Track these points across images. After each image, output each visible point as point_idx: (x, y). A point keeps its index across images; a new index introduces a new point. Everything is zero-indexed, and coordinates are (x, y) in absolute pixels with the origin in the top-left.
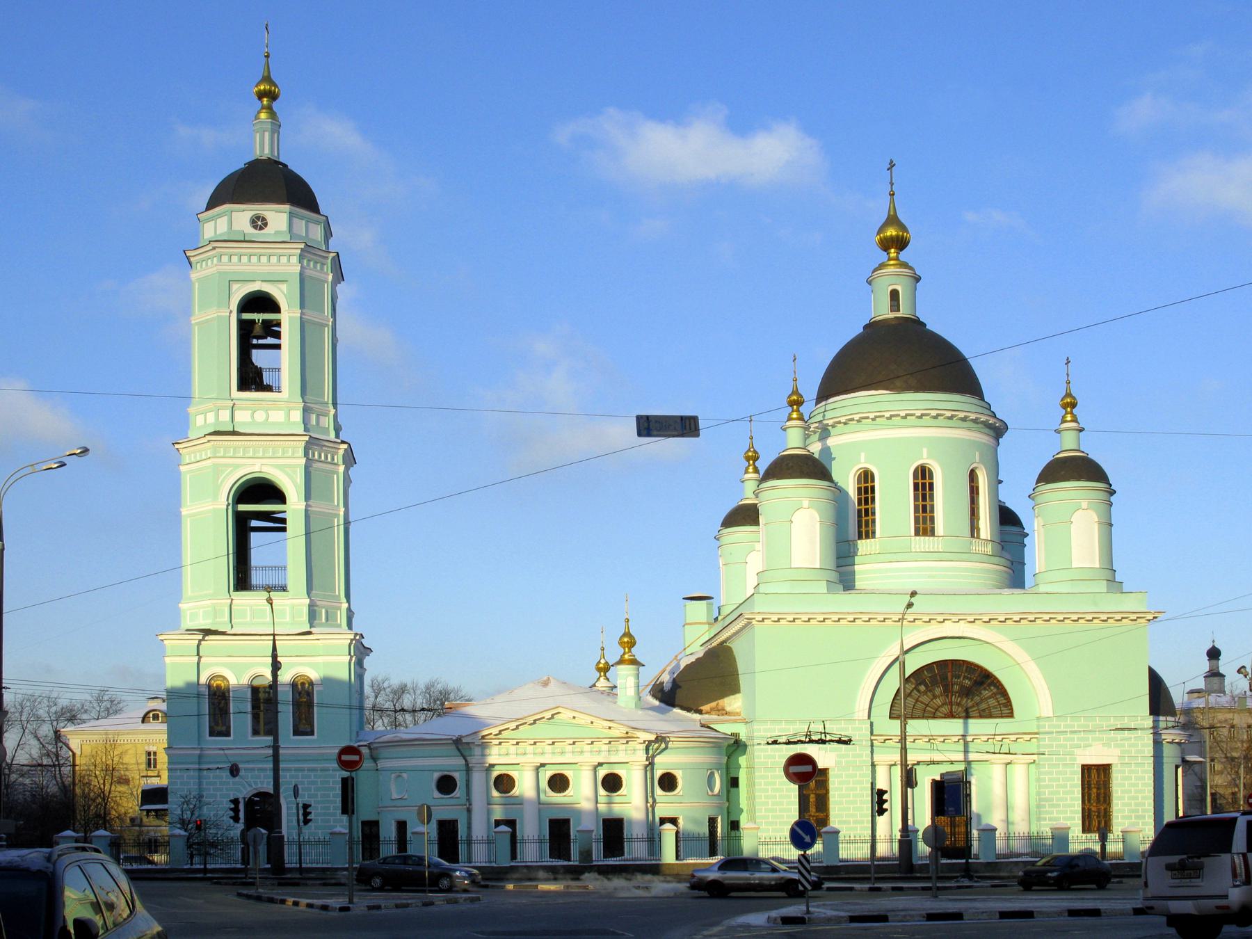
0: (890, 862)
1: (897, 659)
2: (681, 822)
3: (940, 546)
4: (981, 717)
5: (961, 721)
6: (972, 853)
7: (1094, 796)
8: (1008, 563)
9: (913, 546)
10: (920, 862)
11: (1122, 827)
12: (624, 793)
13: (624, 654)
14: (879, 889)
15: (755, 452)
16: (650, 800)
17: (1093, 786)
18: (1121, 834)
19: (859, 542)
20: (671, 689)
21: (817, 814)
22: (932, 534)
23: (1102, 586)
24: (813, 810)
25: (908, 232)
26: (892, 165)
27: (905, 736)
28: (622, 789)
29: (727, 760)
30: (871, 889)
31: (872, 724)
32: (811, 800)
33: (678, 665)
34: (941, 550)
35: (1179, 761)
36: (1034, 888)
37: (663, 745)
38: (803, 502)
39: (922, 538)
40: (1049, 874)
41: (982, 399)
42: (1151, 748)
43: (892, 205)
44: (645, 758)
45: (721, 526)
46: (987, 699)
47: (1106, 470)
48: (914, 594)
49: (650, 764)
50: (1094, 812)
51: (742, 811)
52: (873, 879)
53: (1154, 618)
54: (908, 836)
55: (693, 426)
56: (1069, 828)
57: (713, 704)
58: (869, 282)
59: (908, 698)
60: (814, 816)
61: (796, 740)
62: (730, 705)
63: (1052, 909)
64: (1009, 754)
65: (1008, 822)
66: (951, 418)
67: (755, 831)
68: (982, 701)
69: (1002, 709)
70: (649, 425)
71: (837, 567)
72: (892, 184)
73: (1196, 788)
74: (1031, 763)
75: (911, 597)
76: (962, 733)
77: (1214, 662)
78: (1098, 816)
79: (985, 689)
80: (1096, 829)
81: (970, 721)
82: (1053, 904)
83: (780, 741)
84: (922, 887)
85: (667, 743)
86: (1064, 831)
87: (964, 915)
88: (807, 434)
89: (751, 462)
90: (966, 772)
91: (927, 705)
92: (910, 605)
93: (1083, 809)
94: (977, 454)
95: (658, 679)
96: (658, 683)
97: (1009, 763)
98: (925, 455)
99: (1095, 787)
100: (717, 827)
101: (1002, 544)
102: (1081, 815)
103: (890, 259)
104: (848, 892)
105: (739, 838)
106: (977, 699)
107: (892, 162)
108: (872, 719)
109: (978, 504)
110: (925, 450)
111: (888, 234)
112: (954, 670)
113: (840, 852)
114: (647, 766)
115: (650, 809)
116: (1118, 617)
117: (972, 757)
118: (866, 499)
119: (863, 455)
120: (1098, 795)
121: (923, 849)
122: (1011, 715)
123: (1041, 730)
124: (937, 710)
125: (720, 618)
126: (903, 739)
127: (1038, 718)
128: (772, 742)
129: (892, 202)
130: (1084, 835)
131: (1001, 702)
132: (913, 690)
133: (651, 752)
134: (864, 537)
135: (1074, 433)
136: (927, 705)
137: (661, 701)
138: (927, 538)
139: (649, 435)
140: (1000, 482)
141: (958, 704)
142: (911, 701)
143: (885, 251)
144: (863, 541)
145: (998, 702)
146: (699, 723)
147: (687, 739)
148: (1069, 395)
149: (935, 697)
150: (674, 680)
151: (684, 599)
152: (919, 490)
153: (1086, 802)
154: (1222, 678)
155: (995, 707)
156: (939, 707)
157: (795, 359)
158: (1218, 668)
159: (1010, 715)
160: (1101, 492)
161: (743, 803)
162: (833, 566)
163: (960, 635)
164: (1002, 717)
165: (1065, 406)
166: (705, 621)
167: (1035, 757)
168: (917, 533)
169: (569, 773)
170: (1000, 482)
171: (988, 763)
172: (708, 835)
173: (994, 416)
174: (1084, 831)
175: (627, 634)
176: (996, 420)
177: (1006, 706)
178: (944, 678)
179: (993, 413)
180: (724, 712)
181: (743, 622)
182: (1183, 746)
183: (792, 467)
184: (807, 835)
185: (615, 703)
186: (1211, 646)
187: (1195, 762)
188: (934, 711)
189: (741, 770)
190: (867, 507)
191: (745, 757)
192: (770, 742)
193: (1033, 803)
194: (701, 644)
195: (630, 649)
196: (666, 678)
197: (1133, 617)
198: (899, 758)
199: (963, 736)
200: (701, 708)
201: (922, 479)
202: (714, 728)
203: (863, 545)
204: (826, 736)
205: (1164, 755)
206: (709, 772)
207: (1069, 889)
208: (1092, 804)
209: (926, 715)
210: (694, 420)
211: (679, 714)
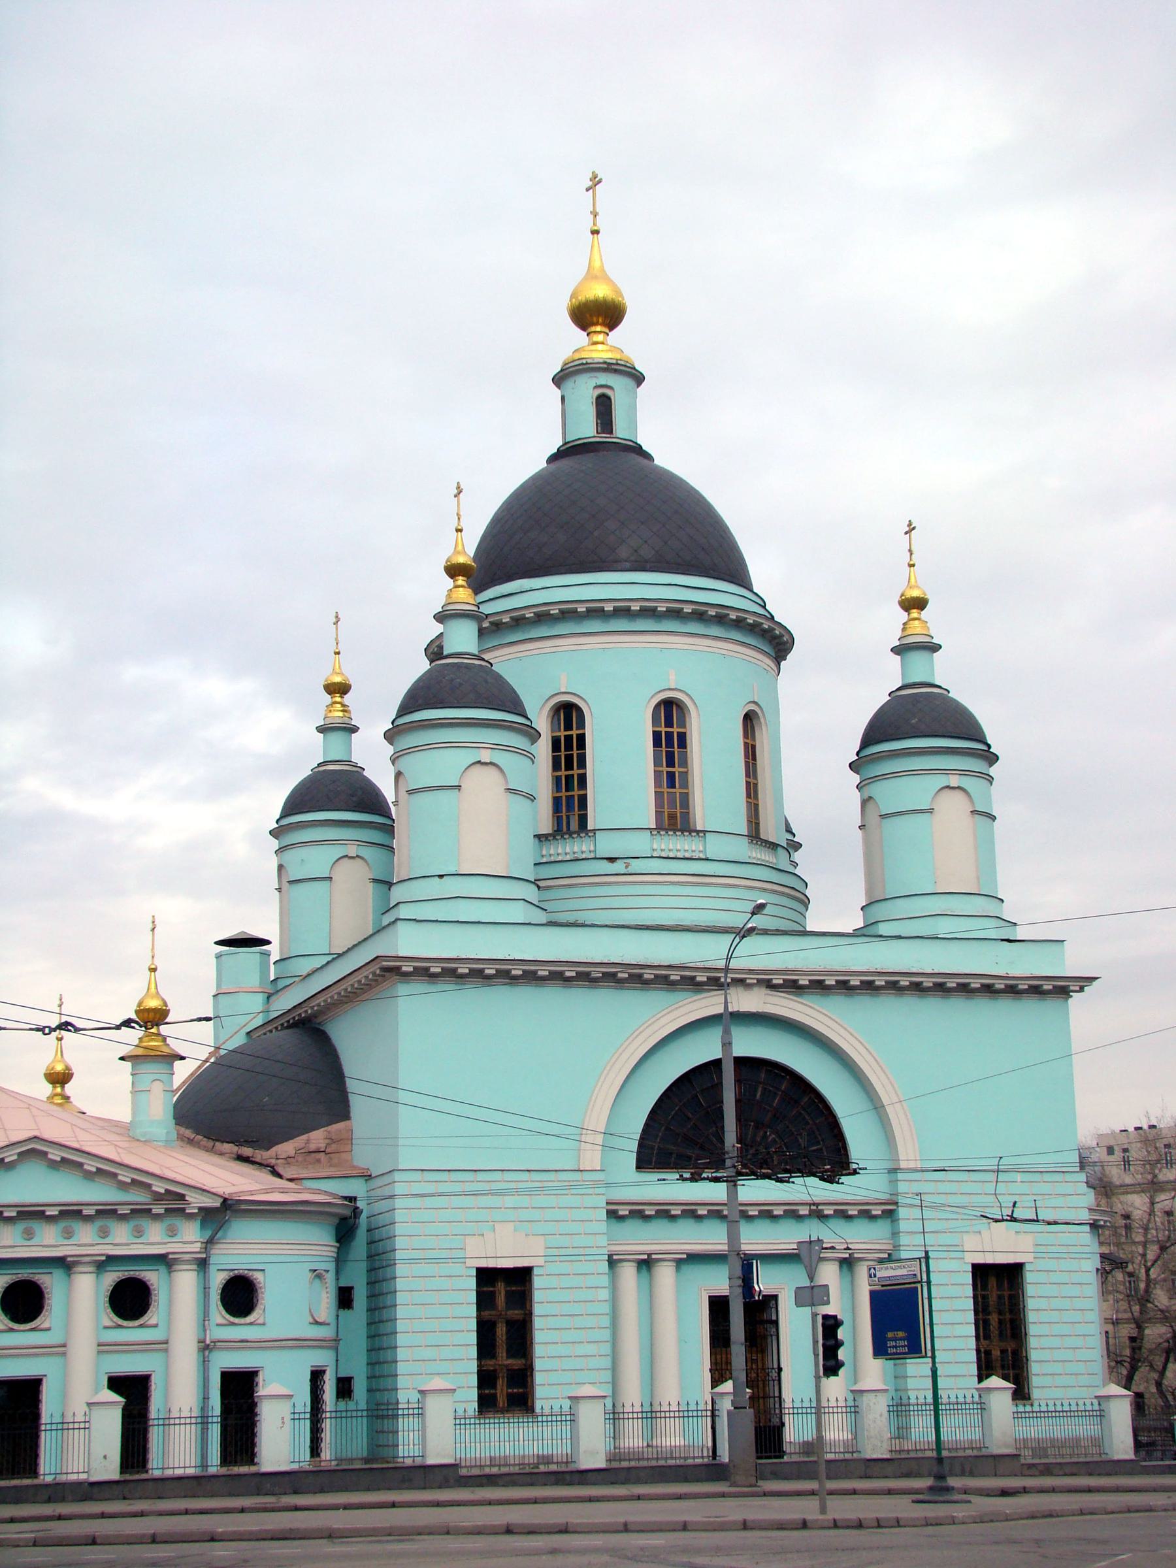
12: (153, 1321)
18: (977, 1393)
24: (502, 1352)
26: (596, 181)
28: (149, 1313)
72: (595, 214)
107: (595, 176)
151: (220, 943)
157: (460, 492)
190: (570, 772)
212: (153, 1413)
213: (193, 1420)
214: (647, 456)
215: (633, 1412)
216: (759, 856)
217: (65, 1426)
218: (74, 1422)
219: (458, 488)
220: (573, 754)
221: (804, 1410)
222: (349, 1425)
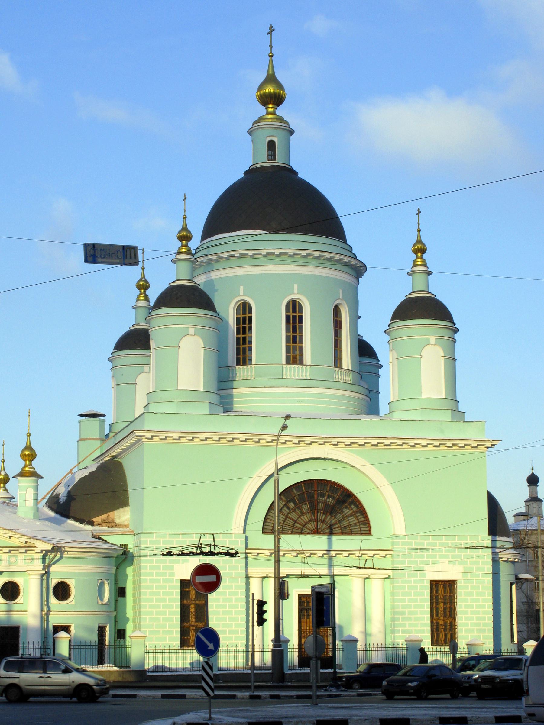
0: (263, 671)
1: (272, 475)
2: (72, 629)
3: (308, 374)
4: (343, 533)
5: (326, 537)
7: (441, 610)
8: (366, 392)
9: (284, 373)
10: (290, 672)
13: (25, 466)
14: (258, 697)
15: (146, 281)
16: (45, 608)
17: (440, 601)
18: (466, 647)
19: (237, 367)
20: (66, 500)
21: (197, 624)
22: (301, 363)
23: (447, 415)
24: (192, 619)
25: (284, 90)
26: (271, 30)
27: (279, 550)
28: (20, 597)
29: (116, 570)
30: (252, 697)
31: (247, 538)
32: (191, 610)
33: (73, 478)
35: (513, 579)
36: (396, 697)
37: (59, 555)
38: (190, 329)
39: (293, 366)
40: (410, 684)
41: (345, 242)
42: (490, 566)
43: (270, 65)
44: (42, 567)
45: (114, 349)
46: (348, 517)
48: (288, 417)
49: (46, 573)
50: (442, 625)
51: (128, 620)
52: (253, 687)
53: (493, 445)
54: (280, 646)
55: (133, 256)
56: (422, 640)
57: (104, 516)
60: (193, 626)
61: (188, 552)
62: (120, 517)
63: (426, 717)
64: (373, 568)
65: (366, 634)
66: (318, 258)
67: (142, 640)
68: (344, 518)
69: (362, 526)
70: (95, 252)
71: (218, 390)
72: (271, 47)
73: (523, 605)
74: (387, 578)
75: (285, 420)
76: (326, 548)
77: (533, 487)
78: (445, 630)
79: (346, 508)
80: (443, 642)
81: (334, 537)
82: (422, 712)
83: (174, 552)
84: (297, 696)
85: (62, 553)
86: (417, 642)
87: (349, 721)
88: (193, 267)
89: (142, 291)
90: (332, 586)
92: (284, 428)
93: (432, 622)
94: (341, 291)
95: (54, 491)
96: (54, 495)
97: (367, 578)
98: (296, 291)
99: (442, 602)
100: (105, 636)
101: (360, 373)
102: (430, 628)
103: (268, 113)
104: (231, 700)
105: (124, 647)
106: (339, 516)
107: (271, 27)
108: (247, 533)
109: (341, 337)
110: (296, 286)
111: (267, 91)
112: (319, 489)
113: (219, 661)
114: (43, 574)
115: (45, 617)
116: (461, 444)
117: (336, 571)
118: (244, 329)
119: (242, 288)
120: (445, 609)
121: (293, 656)
122: (369, 533)
123: (395, 547)
124: (304, 526)
125: (111, 435)
126: (276, 552)
127: (393, 536)
128: (167, 553)
129: (271, 63)
130: (435, 647)
131: (360, 520)
132: (283, 507)
133: (47, 561)
134: (241, 364)
135: (423, 276)
137: (57, 512)
138: (297, 366)
139: (94, 262)
140: (359, 317)
141: (323, 521)
142: (282, 517)
143: (264, 106)
144: (241, 367)
145: (358, 520)
146: (91, 534)
147: (80, 550)
148: (419, 241)
149: (303, 514)
150: (69, 492)
151: (79, 415)
152: (290, 323)
153: (435, 615)
154: (540, 503)
156: (306, 523)
157: (185, 199)
158: (537, 493)
159: (368, 532)
160: (447, 329)
161: (130, 613)
162: (213, 388)
163: (326, 457)
165: (416, 251)
166: (98, 437)
167: (390, 572)
168: (288, 362)
169: (19, 581)
170: (359, 317)
171: (348, 577)
172: (97, 644)
173: (355, 257)
174: (432, 644)
175: (29, 447)
176: (356, 262)
177: (364, 524)
178: (311, 497)
179: (355, 255)
180: (114, 524)
181: (133, 439)
182: (516, 564)
183: (181, 296)
184: (211, 643)
185: (15, 513)
186: (531, 473)
187: (527, 580)
188: (302, 527)
189: (128, 579)
191: (131, 567)
192: (165, 553)
193: (389, 616)
194: (93, 459)
195: (31, 461)
196: (62, 491)
197: (474, 444)
198: (273, 571)
199: (327, 551)
200: (93, 520)
201: (293, 312)
202: (105, 539)
203: (242, 371)
204: (215, 549)
205: (501, 573)
206: (100, 581)
207: (426, 699)
208: (439, 619)
209: (294, 530)
210: (134, 249)
211: (73, 525)
212: (21, 644)
213: (39, 647)
214: (296, 173)
215: (369, 648)
216: (108, 457)
217: (25, 648)
218: (28, 646)
219: (185, 196)
220: (246, 326)
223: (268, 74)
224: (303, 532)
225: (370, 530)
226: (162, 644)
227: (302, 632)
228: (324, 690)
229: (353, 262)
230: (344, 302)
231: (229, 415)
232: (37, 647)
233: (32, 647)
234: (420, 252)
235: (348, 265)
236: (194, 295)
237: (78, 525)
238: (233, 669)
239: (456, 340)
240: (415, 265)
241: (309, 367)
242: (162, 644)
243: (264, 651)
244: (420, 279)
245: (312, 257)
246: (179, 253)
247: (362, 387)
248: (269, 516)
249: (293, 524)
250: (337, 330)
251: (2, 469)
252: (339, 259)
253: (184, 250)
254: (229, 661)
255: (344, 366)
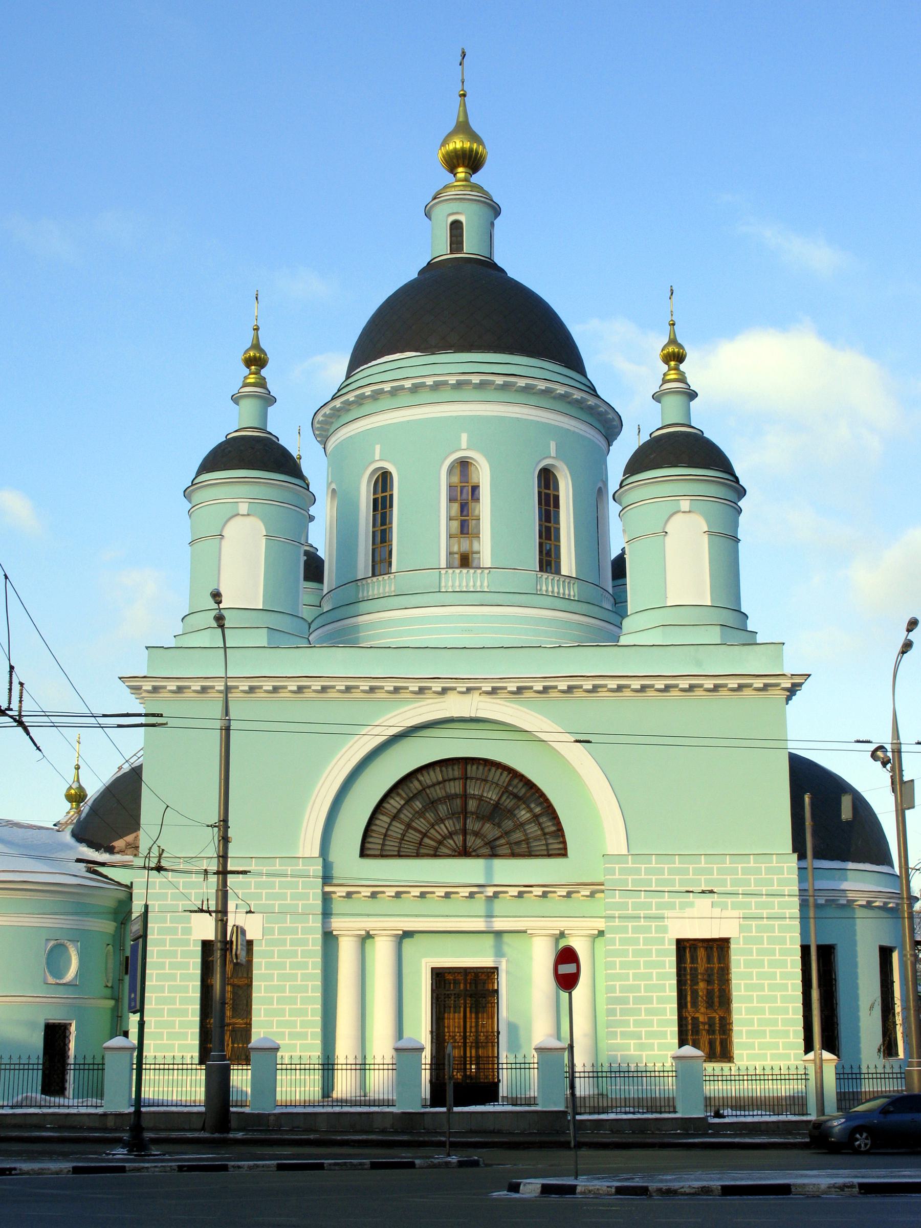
3: (486, 584)
4: (514, 855)
6: (501, 1095)
9: (443, 584)
11: (673, 1052)
34: (486, 590)
47: (729, 457)
58: (428, 215)
59: (394, 823)
69: (550, 841)
91: (425, 835)
94: (553, 445)
110: (464, 437)
119: (378, 447)
120: (710, 994)
122: (563, 853)
136: (425, 835)
141: (476, 834)
145: (542, 829)
155: (536, 839)
164: (549, 856)
177: (557, 837)
183: (230, 452)
206: (51, 943)
209: (422, 851)
221: (846, 1076)
222: (26, 1076)
223: (458, 122)
224: (438, 853)
225: (565, 849)
226: (759, 1065)
227: (446, 1037)
228: (136, 1155)
229: (592, 401)
230: (565, 468)
231: (298, 647)
232: (381, 1067)
233: (344, 1067)
234: (672, 359)
235: (579, 404)
236: (253, 448)
237: (90, 853)
238: (179, 1103)
239: (741, 510)
240: (665, 381)
241: (486, 571)
242: (759, 1065)
243: (365, 1069)
244: (673, 403)
245: (493, 387)
246: (245, 385)
247: (596, 607)
248: (376, 825)
249: (419, 839)
250: (550, 511)
251: (76, 780)
252: (544, 388)
253: (252, 381)
254: (289, 1089)
255: (564, 571)
